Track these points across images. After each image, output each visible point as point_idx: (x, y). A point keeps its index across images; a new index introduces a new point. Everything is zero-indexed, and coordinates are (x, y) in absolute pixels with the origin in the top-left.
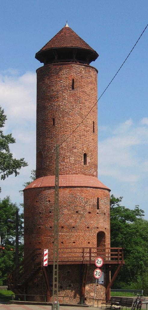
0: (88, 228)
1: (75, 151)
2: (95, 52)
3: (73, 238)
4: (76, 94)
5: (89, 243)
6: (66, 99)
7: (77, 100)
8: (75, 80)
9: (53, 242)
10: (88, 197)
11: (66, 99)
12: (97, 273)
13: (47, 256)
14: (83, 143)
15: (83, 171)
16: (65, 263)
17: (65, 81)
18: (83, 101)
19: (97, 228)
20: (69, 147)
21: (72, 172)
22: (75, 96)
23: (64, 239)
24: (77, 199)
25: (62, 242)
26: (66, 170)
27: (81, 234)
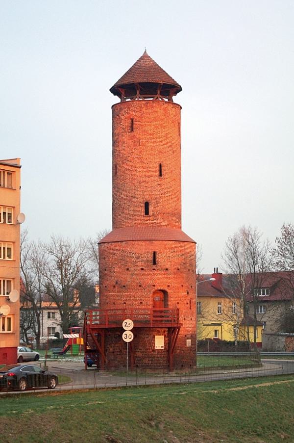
0: (140, 286)
2: (180, 86)
5: (141, 303)
7: (137, 143)
8: (134, 120)
19: (154, 286)
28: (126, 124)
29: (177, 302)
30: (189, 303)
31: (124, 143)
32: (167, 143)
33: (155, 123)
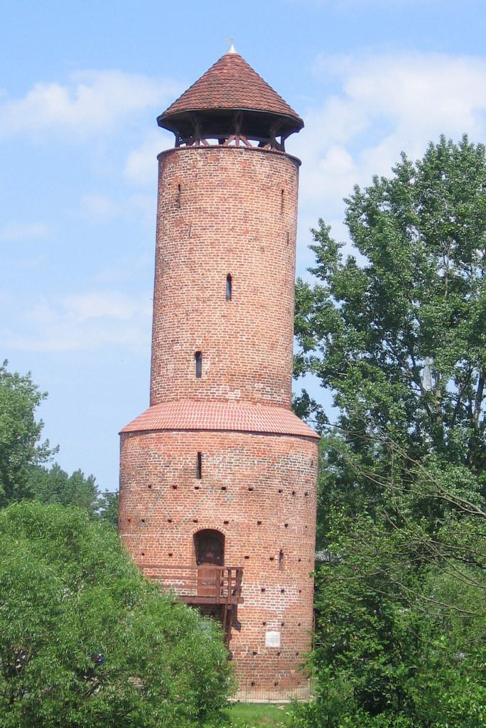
0: (170, 521)
1: (177, 348)
5: (171, 555)
10: (171, 453)
18: (199, 232)
19: (196, 521)
28: (171, 193)
29: (245, 554)
30: (277, 557)
32: (247, 232)
33: (219, 192)
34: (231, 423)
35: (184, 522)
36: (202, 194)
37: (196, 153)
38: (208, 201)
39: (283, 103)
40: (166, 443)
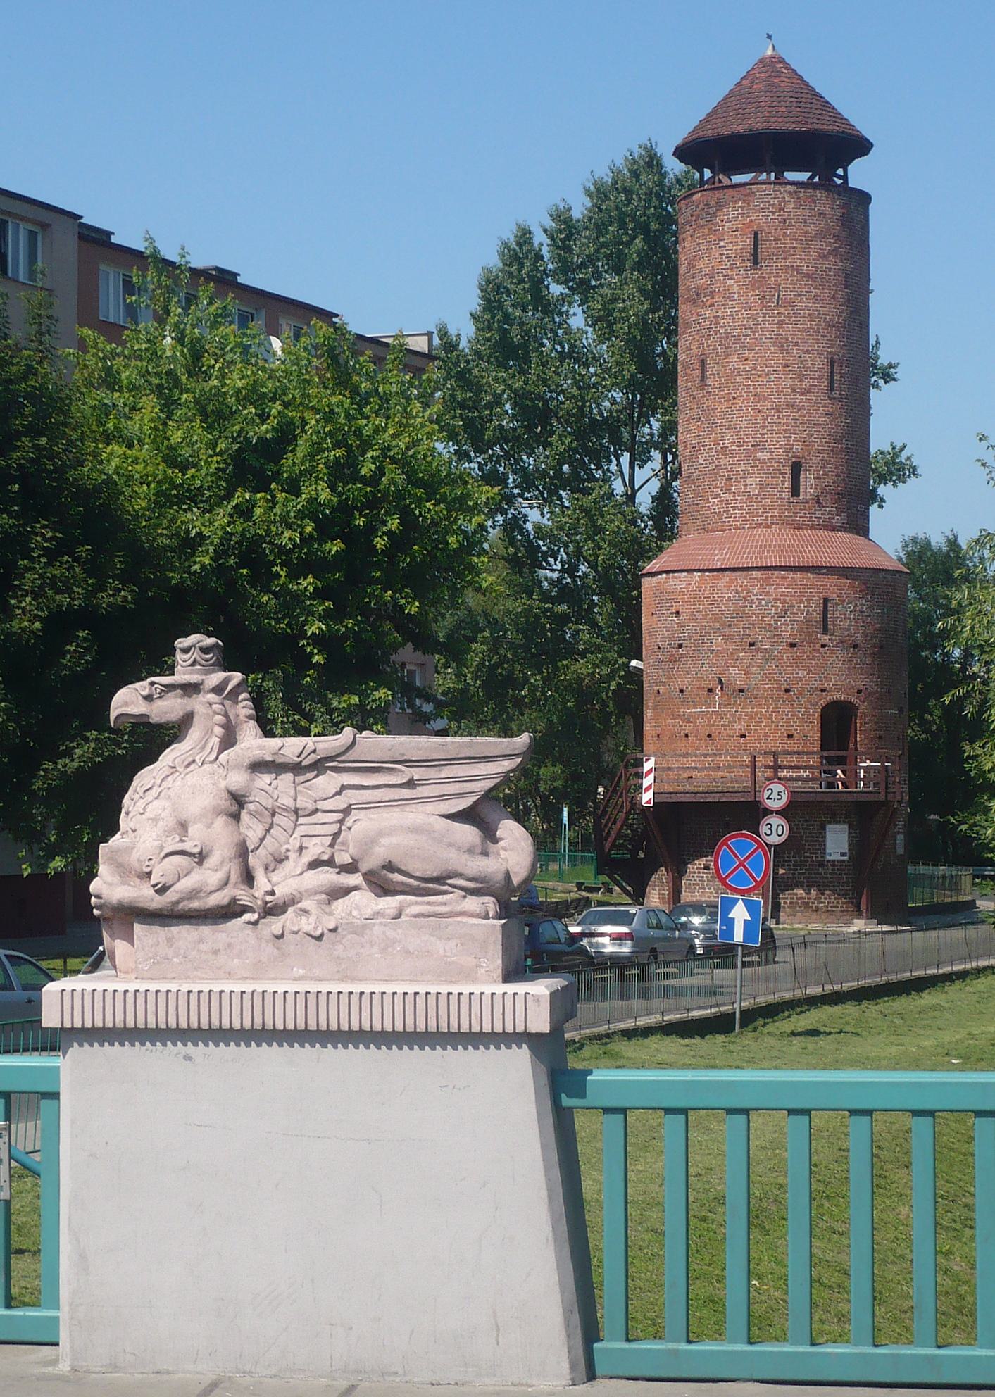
0: (787, 691)
3: (740, 723)
4: (764, 277)
5: (790, 736)
6: (736, 296)
9: (687, 736)
11: (736, 296)
12: (770, 829)
13: (651, 776)
14: (789, 430)
15: (791, 516)
16: (702, 798)
17: (731, 242)
20: (743, 446)
21: (753, 520)
22: (762, 286)
23: (713, 725)
24: (751, 607)
25: (709, 736)
26: (735, 517)
27: (763, 710)
31: (730, 299)
34: (775, 557)
35: (808, 691)
36: (794, 248)
37: (782, 190)
38: (803, 257)
39: (845, 121)
40: (778, 585)
